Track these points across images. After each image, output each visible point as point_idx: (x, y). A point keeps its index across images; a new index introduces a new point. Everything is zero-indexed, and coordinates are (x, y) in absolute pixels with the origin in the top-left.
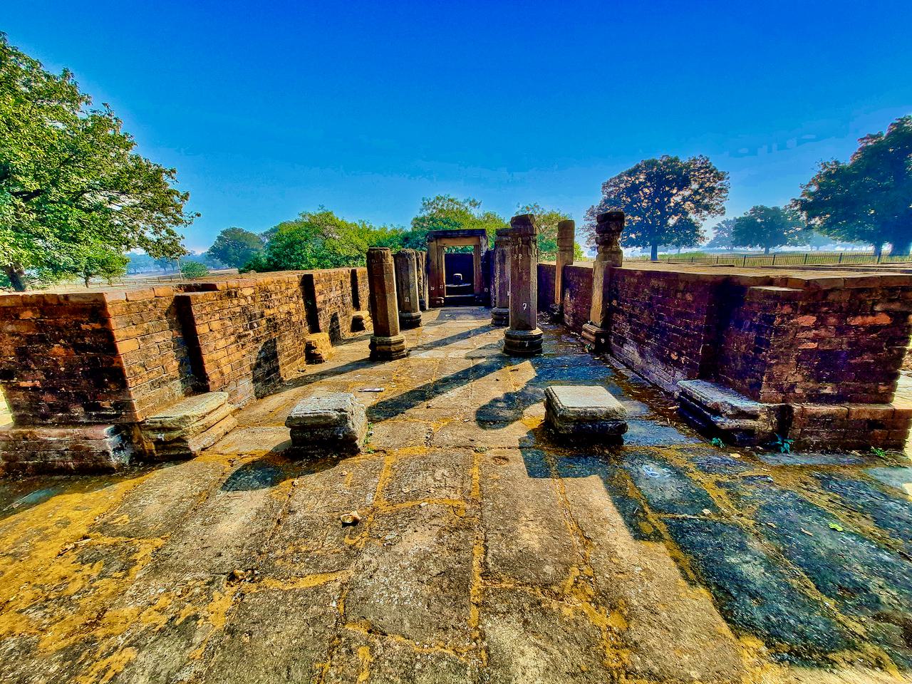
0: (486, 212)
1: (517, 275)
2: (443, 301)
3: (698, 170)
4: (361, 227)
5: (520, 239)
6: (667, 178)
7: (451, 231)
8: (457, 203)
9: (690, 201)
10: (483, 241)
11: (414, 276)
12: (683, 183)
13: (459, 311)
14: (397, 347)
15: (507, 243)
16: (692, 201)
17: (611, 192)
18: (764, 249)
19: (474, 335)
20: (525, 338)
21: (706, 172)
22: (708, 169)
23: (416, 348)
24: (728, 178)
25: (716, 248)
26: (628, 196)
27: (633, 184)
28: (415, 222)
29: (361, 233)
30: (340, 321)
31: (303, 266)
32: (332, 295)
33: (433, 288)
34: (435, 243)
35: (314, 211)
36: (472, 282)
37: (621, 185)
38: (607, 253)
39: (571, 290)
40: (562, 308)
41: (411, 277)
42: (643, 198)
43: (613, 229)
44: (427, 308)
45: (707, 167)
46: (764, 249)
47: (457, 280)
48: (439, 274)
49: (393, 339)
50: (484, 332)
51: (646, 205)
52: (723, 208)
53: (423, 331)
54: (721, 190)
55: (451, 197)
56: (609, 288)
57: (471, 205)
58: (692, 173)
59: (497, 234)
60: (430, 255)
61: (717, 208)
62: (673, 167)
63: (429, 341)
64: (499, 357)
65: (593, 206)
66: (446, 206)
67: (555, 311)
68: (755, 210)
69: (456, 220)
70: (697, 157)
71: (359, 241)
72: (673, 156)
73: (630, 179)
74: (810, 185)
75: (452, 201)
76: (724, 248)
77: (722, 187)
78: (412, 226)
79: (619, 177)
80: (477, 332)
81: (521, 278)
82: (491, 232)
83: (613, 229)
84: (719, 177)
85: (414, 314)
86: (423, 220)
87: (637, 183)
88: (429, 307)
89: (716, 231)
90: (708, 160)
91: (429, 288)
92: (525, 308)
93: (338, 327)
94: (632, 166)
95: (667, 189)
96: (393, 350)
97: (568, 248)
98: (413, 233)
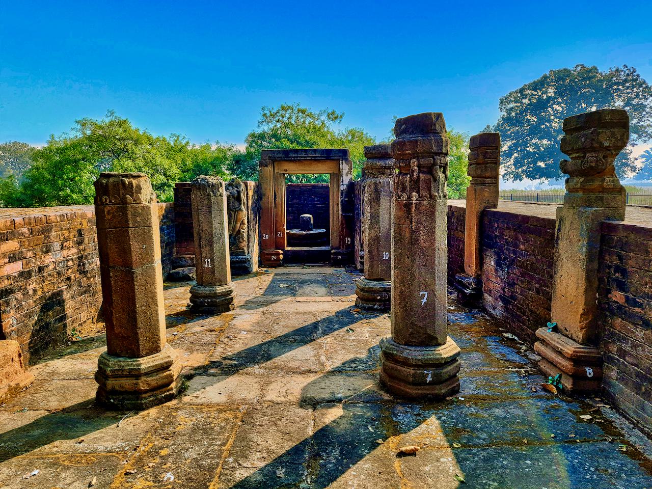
0: (350, 129)
1: (407, 234)
2: (281, 256)
4: (172, 144)
5: (414, 163)
7: (296, 151)
8: (310, 115)
10: (344, 167)
11: (221, 223)
13: (304, 277)
14: (153, 380)
15: (382, 171)
17: (512, 109)
19: (325, 333)
20: (426, 365)
21: (633, 87)
23: (203, 370)
25: (645, 181)
26: (532, 114)
27: (539, 99)
28: (250, 139)
29: (172, 152)
30: (69, 305)
31: (75, 196)
32: (49, 259)
33: (266, 237)
34: (270, 168)
35: (103, 119)
36: (327, 227)
37: (524, 101)
38: (592, 191)
39: (497, 254)
40: (478, 280)
41: (216, 225)
42: (552, 117)
44: (255, 268)
45: (636, 80)
47: (305, 225)
48: (276, 215)
49: (146, 363)
50: (343, 325)
51: (556, 125)
53: (234, 322)
55: (302, 107)
56: (600, 264)
57: (329, 118)
59: (366, 154)
60: (264, 186)
63: (238, 347)
64: (370, 400)
65: (488, 126)
66: (294, 118)
67: (466, 287)
69: (308, 137)
70: (621, 68)
71: (166, 163)
72: (589, 65)
73: (535, 93)
75: (303, 112)
78: (246, 145)
79: (521, 91)
80: (331, 324)
81: (414, 241)
82: (356, 152)
83: (606, 144)
85: (220, 289)
86: (262, 137)
87: (545, 97)
88: (260, 265)
89: (644, 160)
90: (634, 71)
91: (260, 236)
92: (424, 301)
93: (64, 318)
94: (538, 78)
95: (584, 105)
96: (143, 387)
97: (488, 180)
98: (249, 156)
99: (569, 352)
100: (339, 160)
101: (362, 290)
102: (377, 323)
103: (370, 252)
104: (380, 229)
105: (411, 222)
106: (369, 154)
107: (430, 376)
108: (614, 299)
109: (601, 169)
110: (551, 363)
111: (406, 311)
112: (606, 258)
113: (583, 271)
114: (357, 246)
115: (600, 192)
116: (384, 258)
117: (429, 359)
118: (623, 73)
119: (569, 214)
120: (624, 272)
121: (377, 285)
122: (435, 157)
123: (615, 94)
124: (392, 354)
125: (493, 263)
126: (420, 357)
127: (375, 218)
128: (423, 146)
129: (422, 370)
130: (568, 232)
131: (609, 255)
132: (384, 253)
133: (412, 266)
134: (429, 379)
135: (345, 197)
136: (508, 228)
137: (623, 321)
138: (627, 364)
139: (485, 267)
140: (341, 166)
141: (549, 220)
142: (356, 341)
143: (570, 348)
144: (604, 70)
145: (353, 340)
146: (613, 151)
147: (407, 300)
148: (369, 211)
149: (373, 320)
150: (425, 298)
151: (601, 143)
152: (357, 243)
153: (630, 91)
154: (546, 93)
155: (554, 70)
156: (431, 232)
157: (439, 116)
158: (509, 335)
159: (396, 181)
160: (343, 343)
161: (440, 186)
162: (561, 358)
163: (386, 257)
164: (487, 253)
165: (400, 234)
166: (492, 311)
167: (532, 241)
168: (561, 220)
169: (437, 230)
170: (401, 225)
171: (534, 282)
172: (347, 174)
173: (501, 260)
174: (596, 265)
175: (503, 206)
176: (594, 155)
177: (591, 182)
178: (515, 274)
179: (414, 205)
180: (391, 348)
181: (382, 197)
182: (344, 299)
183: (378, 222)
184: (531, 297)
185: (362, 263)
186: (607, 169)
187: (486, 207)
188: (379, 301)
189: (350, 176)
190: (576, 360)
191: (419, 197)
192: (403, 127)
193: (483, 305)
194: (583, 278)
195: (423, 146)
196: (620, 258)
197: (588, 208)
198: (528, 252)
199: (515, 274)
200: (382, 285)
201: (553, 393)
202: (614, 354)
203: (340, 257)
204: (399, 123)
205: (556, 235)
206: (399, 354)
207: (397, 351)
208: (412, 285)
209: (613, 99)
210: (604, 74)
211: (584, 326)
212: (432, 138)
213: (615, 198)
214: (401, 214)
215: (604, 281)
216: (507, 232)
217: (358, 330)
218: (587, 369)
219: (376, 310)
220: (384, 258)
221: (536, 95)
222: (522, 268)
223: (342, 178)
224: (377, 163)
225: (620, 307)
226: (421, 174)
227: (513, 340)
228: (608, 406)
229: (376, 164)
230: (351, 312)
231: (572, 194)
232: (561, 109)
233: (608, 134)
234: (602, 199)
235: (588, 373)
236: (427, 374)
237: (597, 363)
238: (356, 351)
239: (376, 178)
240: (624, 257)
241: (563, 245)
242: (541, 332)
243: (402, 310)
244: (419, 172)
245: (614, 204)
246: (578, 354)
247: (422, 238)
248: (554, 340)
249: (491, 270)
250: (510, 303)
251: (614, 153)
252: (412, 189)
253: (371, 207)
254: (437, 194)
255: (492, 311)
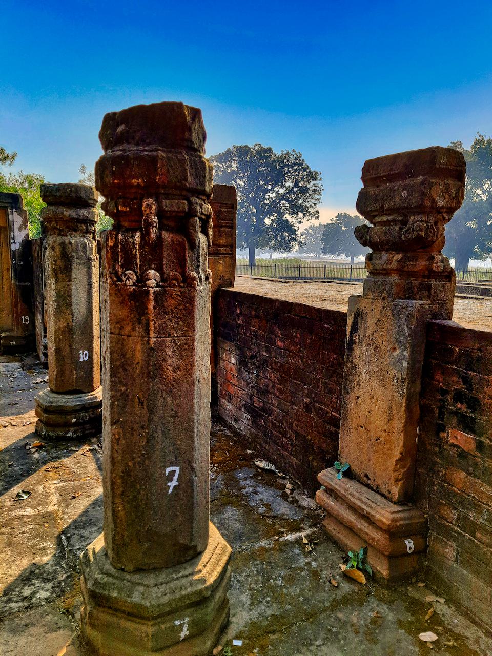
0: (25, 174)
1: (139, 356)
3: (292, 167)
9: (285, 200)
16: (287, 200)
18: (350, 258)
22: (299, 164)
24: (321, 180)
43: (440, 203)
46: (350, 258)
54: (314, 191)
58: (286, 169)
62: (266, 158)
68: (339, 216)
70: (290, 151)
72: (265, 146)
73: (220, 165)
76: (312, 255)
77: (315, 188)
81: (154, 369)
83: (440, 203)
84: (313, 176)
92: (173, 483)
99: (384, 520)
100: (7, 207)
101: (47, 410)
102: (71, 466)
103: (58, 351)
104: (73, 316)
105: (147, 330)
106: (49, 196)
107: (185, 628)
108: (451, 441)
109: (432, 241)
110: (350, 529)
111: (136, 507)
112: (437, 377)
113: (402, 396)
114: (39, 330)
115: (424, 277)
116: (81, 360)
117: (185, 596)
118: (292, 157)
119: (374, 311)
120: (474, 404)
121: (69, 401)
122: (193, 199)
123: (286, 175)
124: (108, 598)
125: (233, 360)
126: (166, 599)
127: (65, 300)
128: (168, 172)
129: (170, 621)
130: (372, 334)
131: (443, 373)
132: (81, 352)
133: (150, 421)
134: (184, 633)
135: (20, 261)
136: (256, 316)
137: (469, 477)
138: (478, 543)
139: (222, 364)
140: (10, 217)
141: (340, 313)
142: (33, 518)
143: (385, 513)
144: (278, 152)
145: (29, 516)
146: (445, 215)
147: (138, 486)
148: (54, 287)
149: (67, 461)
150: (175, 478)
151: (433, 201)
152: (38, 323)
153: (297, 174)
154: (231, 166)
155: (236, 145)
156: (187, 349)
157: (196, 113)
158: (262, 464)
159: (111, 244)
160: (7, 530)
161: (201, 260)
162: (366, 525)
163: (83, 356)
164: (224, 346)
165: (124, 355)
166: (233, 423)
167: (296, 337)
168: (359, 315)
169: (197, 345)
170: (125, 337)
171: (301, 393)
172: (20, 229)
173: (245, 357)
174: (418, 387)
175: (243, 284)
176: (424, 219)
177: (412, 261)
178: (269, 379)
179: (151, 297)
180: (105, 584)
181: (74, 266)
182: (16, 420)
183: (70, 304)
184: (296, 414)
185: (46, 355)
186: (437, 242)
187: (220, 286)
188: (75, 424)
189: (24, 232)
190: (395, 533)
191: (162, 280)
192: (121, 128)
193: (219, 413)
194: (401, 407)
195: (168, 172)
196: (466, 381)
197: (410, 301)
198: (290, 351)
199: (269, 379)
200: (80, 401)
201: (361, 584)
202: (451, 523)
203: (14, 343)
204: (111, 121)
205: (348, 337)
206: (124, 597)
207: (120, 590)
208: (149, 458)
209: (285, 179)
210: (277, 156)
211: (400, 477)
212: (186, 157)
213: (444, 286)
214: (123, 313)
215: (432, 411)
216: (255, 322)
217: (40, 489)
218: (407, 542)
219: (70, 440)
220: (81, 360)
221: (221, 167)
222: (280, 372)
223: (12, 233)
224: (65, 213)
225: (463, 455)
226: (164, 233)
227: (270, 471)
228: (442, 600)
229: (62, 214)
230: (28, 447)
231: (380, 279)
232: (243, 184)
233: (442, 187)
234: (428, 288)
235: (408, 549)
236: (181, 626)
237: (420, 531)
238: (34, 546)
239: (63, 235)
240: (474, 381)
241: (361, 353)
242: (326, 476)
243: (127, 506)
244: (161, 227)
245: (441, 296)
246: (398, 524)
247: (169, 361)
248: (353, 496)
249: (231, 370)
250: (261, 416)
251: (447, 218)
252: (147, 264)
253: (57, 282)
254: (196, 275)
255: (233, 423)
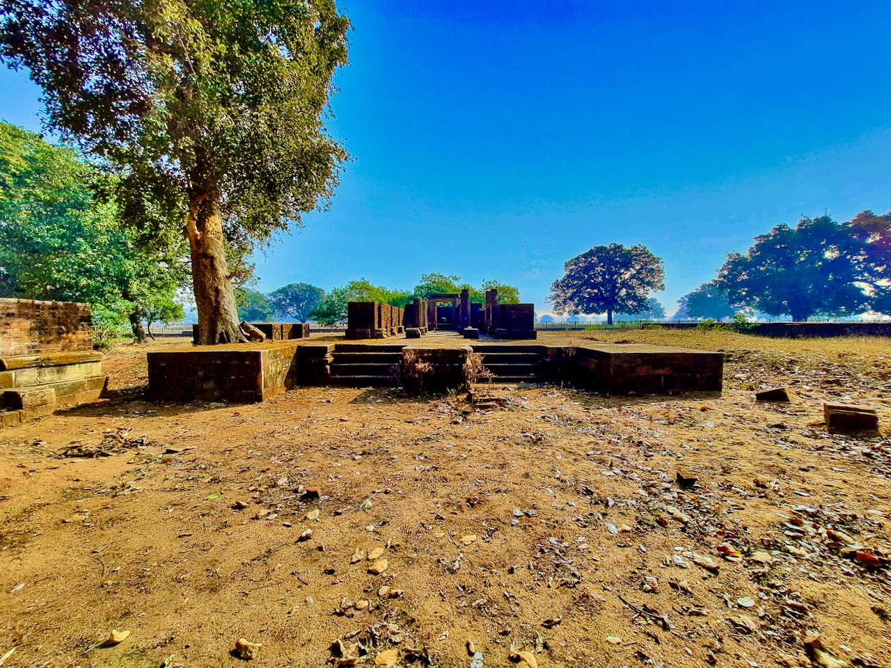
6: (614, 259)
12: (627, 265)
26: (584, 273)
52: (663, 285)
61: (659, 284)
74: (723, 269)
79: (577, 259)
84: (656, 261)
86: (422, 287)
